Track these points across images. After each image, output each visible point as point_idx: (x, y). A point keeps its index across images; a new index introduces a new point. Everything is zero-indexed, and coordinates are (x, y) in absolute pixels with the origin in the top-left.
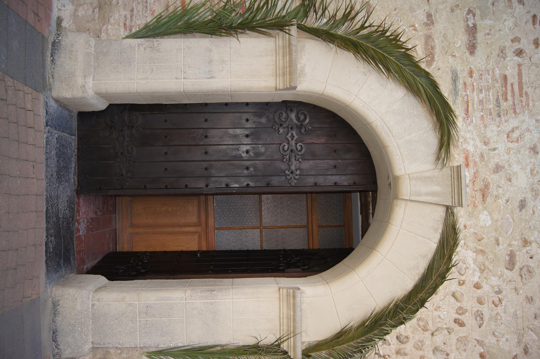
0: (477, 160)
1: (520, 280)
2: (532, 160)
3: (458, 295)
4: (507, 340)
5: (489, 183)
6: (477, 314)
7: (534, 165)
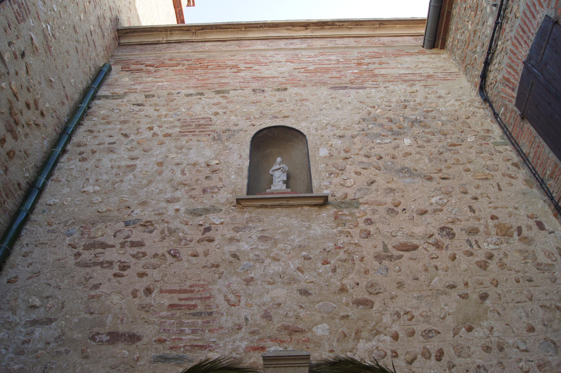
0: (257, 337)
1: (382, 295)
2: (259, 283)
3: (409, 357)
4: (446, 305)
5: (283, 326)
6: (425, 336)
7: (264, 282)
